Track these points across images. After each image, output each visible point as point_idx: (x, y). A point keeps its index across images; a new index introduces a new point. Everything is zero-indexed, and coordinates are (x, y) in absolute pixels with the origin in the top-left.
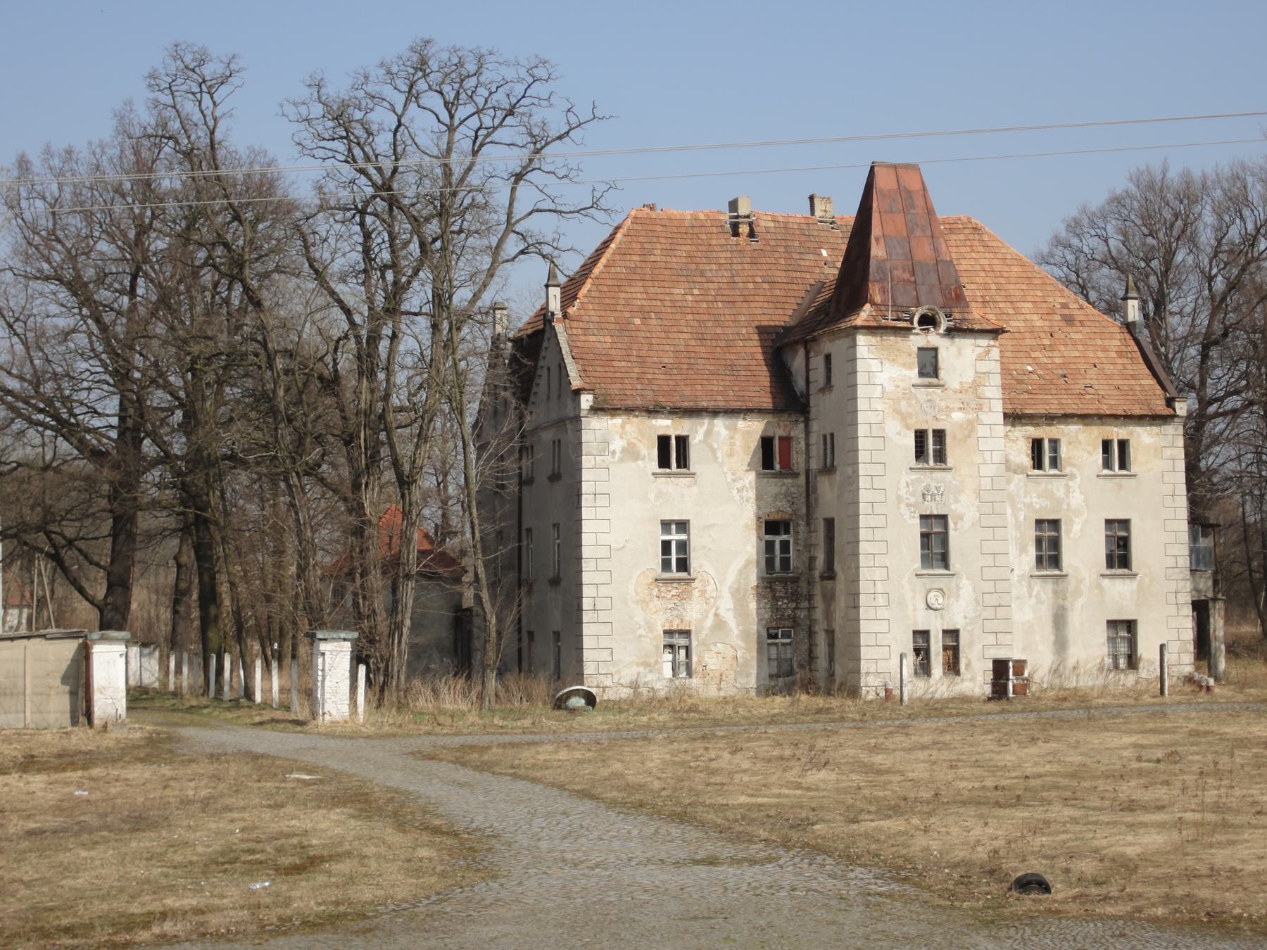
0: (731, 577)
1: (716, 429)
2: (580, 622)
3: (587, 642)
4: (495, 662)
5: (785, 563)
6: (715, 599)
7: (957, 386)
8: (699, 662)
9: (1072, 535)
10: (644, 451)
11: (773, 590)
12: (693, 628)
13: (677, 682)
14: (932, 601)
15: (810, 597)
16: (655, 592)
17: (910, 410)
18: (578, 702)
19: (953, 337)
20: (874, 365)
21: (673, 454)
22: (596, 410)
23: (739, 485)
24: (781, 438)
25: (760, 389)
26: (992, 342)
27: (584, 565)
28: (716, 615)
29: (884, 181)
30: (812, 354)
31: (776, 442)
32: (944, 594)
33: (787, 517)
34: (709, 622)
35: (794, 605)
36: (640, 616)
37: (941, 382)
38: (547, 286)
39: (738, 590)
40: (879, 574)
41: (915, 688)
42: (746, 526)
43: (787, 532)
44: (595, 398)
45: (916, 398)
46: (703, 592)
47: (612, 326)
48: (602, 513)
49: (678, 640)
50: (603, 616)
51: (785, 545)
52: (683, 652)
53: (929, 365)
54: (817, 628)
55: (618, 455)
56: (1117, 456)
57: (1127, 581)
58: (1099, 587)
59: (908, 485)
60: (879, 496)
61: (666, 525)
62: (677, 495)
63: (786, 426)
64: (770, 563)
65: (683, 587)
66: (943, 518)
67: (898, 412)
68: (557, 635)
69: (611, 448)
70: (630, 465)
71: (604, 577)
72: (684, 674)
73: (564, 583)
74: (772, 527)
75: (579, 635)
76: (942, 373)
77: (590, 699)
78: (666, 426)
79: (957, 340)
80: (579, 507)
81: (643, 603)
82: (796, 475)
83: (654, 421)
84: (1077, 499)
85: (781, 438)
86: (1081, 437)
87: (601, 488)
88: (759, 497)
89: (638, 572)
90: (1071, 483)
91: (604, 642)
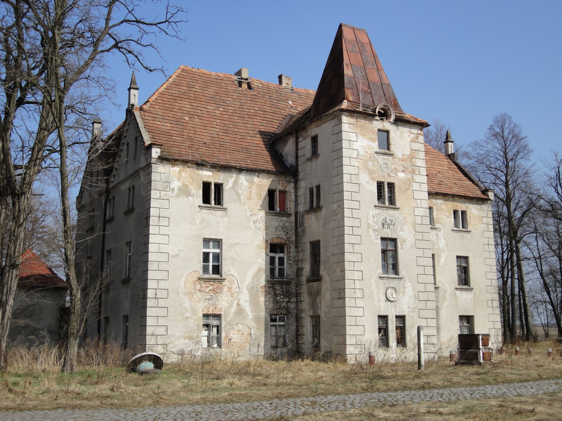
0: (248, 279)
1: (240, 181)
2: (145, 307)
3: (150, 321)
4: (78, 331)
5: (281, 271)
6: (238, 293)
7: (400, 156)
8: (226, 337)
9: (440, 264)
10: (193, 191)
11: (274, 289)
12: (222, 313)
13: (212, 350)
14: (389, 296)
15: (298, 295)
16: (198, 287)
17: (374, 168)
18: (148, 366)
19: (398, 126)
20: (353, 137)
21: (212, 195)
22: (162, 159)
23: (254, 218)
24: (280, 191)
25: (265, 160)
26: (419, 132)
27: (149, 266)
28: (238, 304)
29: (347, 34)
30: (300, 139)
31: (277, 194)
32: (396, 291)
33: (283, 242)
34: (233, 309)
35: (287, 300)
36: (187, 304)
37: (392, 153)
38: (129, 90)
39: (252, 288)
40: (357, 275)
41: (380, 355)
42: (258, 246)
43: (282, 252)
44: (162, 152)
45: (378, 162)
46: (230, 289)
47: (171, 119)
48: (163, 230)
49: (212, 321)
50: (162, 303)
51: (281, 260)
52: (215, 330)
53: (385, 140)
54: (303, 315)
55: (176, 191)
56: (461, 219)
57: (468, 293)
58: (455, 295)
59: (373, 217)
60: (356, 223)
61: (207, 241)
62: (214, 222)
63: (283, 184)
64: (272, 271)
65: (216, 285)
66: (394, 240)
67: (368, 169)
68: (126, 318)
69: (172, 186)
70: (184, 199)
71: (163, 275)
72: (216, 345)
73: (133, 281)
74: (274, 247)
75: (144, 317)
76: (392, 147)
77: (157, 362)
78: (208, 175)
79: (400, 128)
80: (147, 225)
81: (190, 294)
82: (289, 215)
83: (200, 172)
84: (442, 243)
85: (280, 191)
86: (443, 207)
87: (163, 213)
88: (267, 228)
89: (187, 273)
90: (439, 233)
91: (162, 322)
